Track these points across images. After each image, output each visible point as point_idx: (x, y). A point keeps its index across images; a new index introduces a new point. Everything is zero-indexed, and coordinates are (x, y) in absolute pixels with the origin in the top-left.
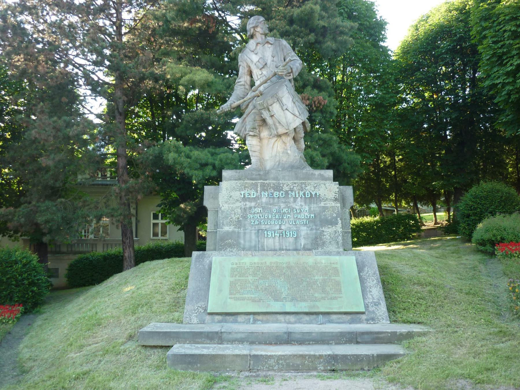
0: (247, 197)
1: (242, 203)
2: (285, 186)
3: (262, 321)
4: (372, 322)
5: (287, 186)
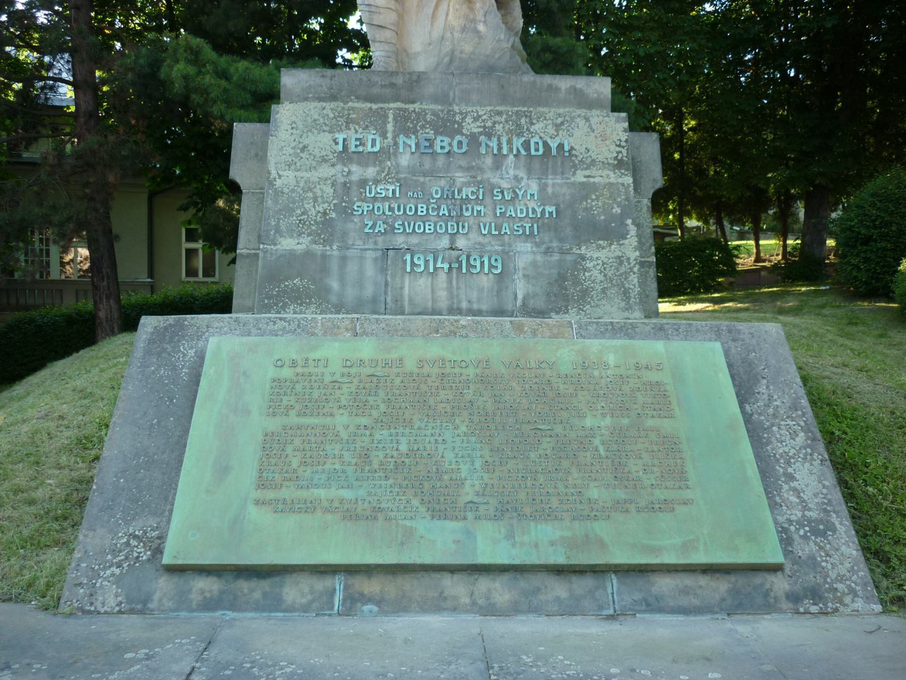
0: (353, 149)
1: (339, 167)
2: (469, 120)
3: (379, 602)
4: (814, 609)
5: (476, 119)
